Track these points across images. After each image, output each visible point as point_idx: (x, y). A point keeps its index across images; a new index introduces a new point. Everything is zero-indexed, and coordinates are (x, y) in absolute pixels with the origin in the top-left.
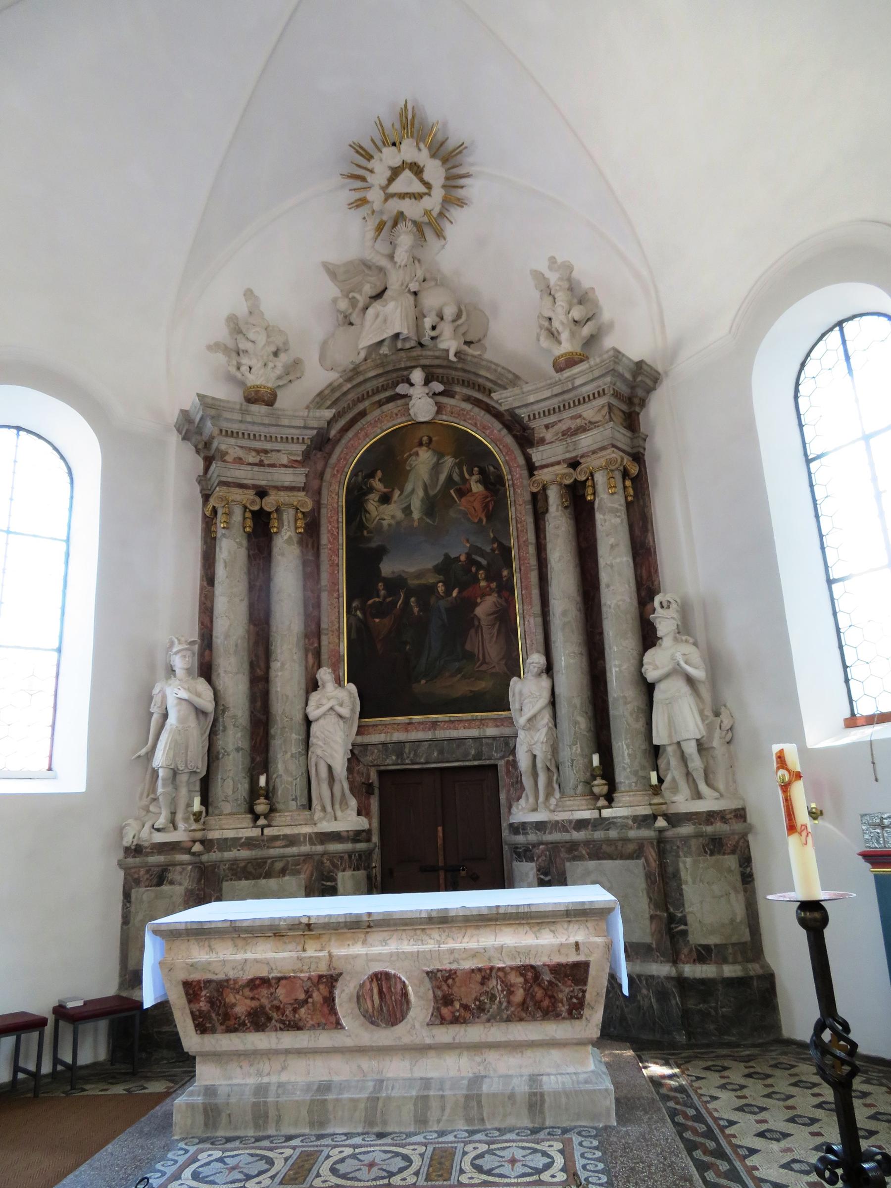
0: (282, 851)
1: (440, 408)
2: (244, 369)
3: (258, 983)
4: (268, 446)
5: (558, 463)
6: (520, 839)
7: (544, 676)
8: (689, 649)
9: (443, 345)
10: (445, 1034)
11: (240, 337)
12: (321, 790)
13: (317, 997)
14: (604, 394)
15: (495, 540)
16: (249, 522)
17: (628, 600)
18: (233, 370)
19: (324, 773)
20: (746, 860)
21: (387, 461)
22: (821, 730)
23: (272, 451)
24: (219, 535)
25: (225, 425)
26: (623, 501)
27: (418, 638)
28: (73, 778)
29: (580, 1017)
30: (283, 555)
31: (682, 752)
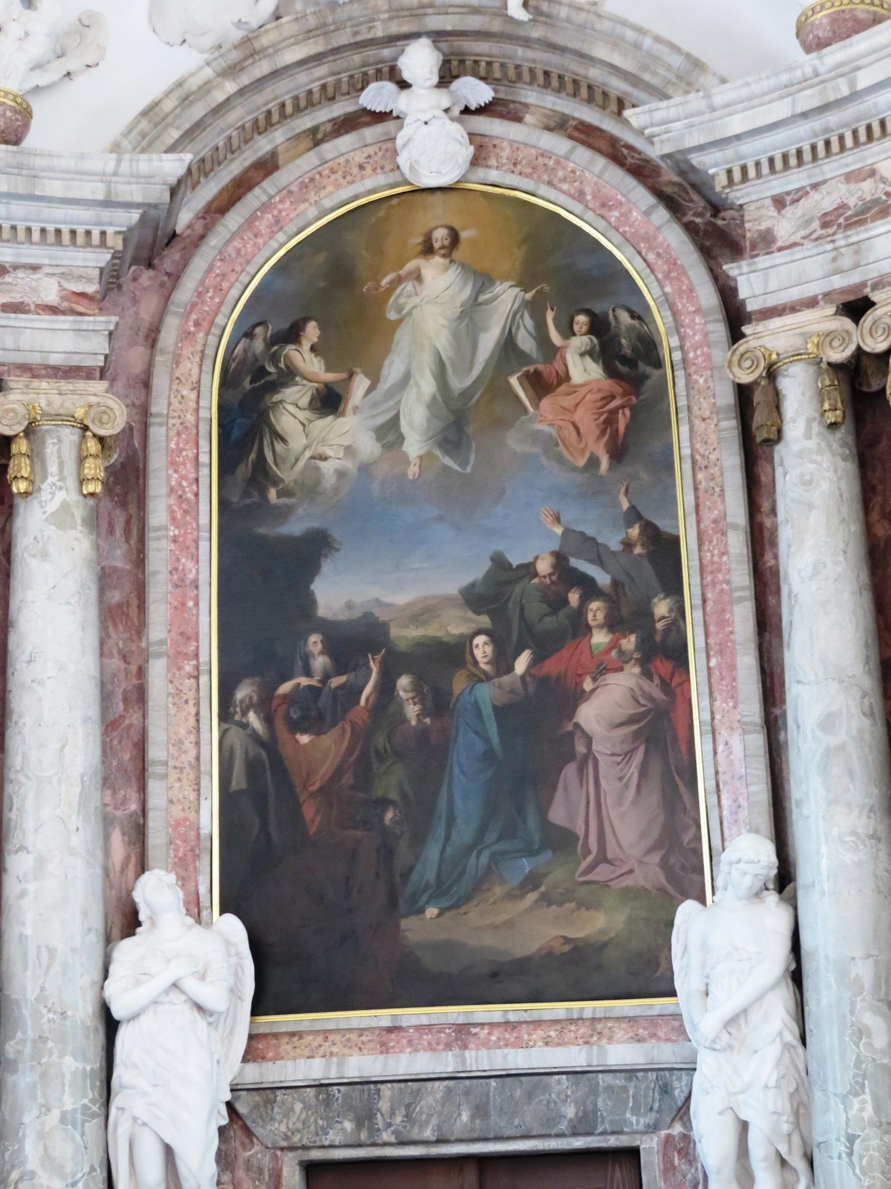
5: (812, 303)
15: (634, 515)
21: (332, 294)
30: (44, 555)
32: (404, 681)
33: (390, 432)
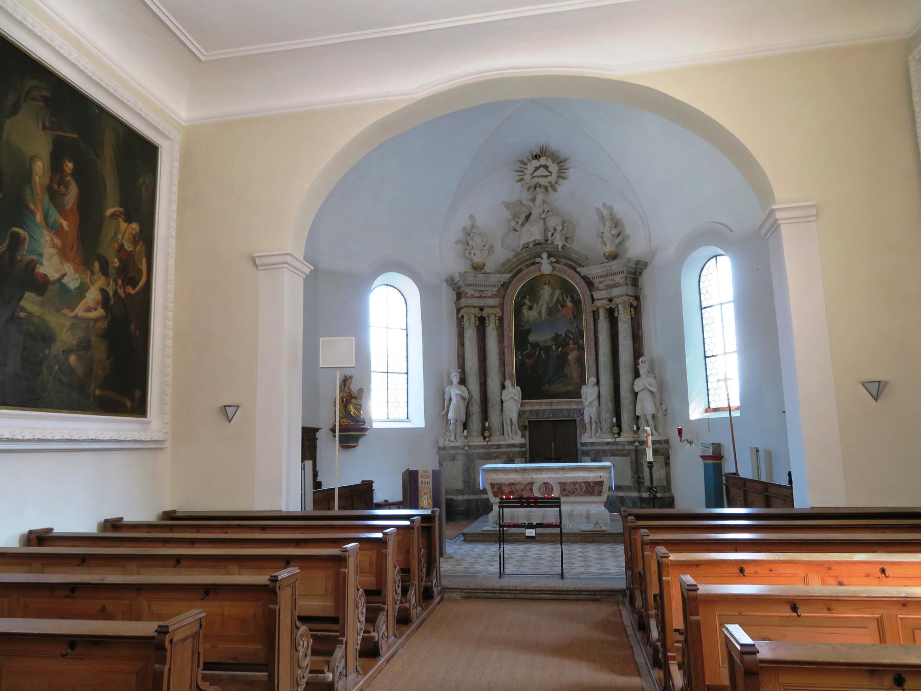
1: (554, 269)
3: (511, 484)
6: (585, 448)
9: (556, 243)
12: (507, 428)
13: (528, 488)
15: (577, 327)
19: (509, 422)
20: (667, 458)
21: (531, 291)
22: (696, 412)
25: (467, 282)
27: (543, 370)
28: (418, 421)
33: (540, 313)
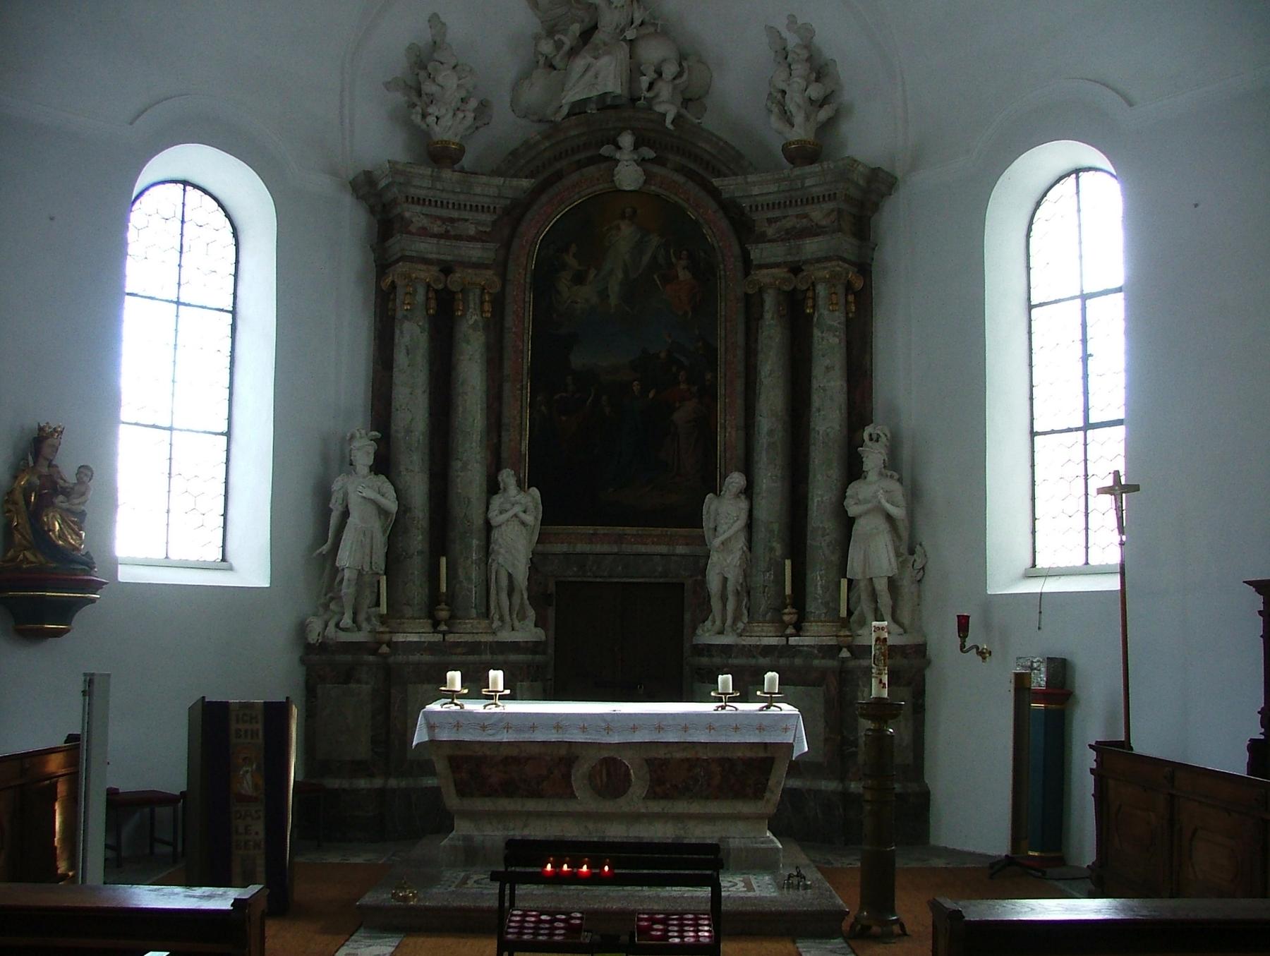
0: (464, 657)
1: (649, 177)
2: (431, 120)
4: (455, 214)
5: (777, 265)
7: (743, 497)
8: (895, 486)
9: (660, 108)
10: (655, 807)
11: (423, 74)
14: (835, 198)
16: (433, 303)
17: (838, 428)
18: (417, 119)
19: (504, 582)
21: (583, 232)
23: (459, 220)
24: (399, 314)
25: (412, 191)
26: (843, 319)
28: (252, 569)
29: (762, 798)
30: (468, 342)
31: (874, 589)
32: (604, 398)
